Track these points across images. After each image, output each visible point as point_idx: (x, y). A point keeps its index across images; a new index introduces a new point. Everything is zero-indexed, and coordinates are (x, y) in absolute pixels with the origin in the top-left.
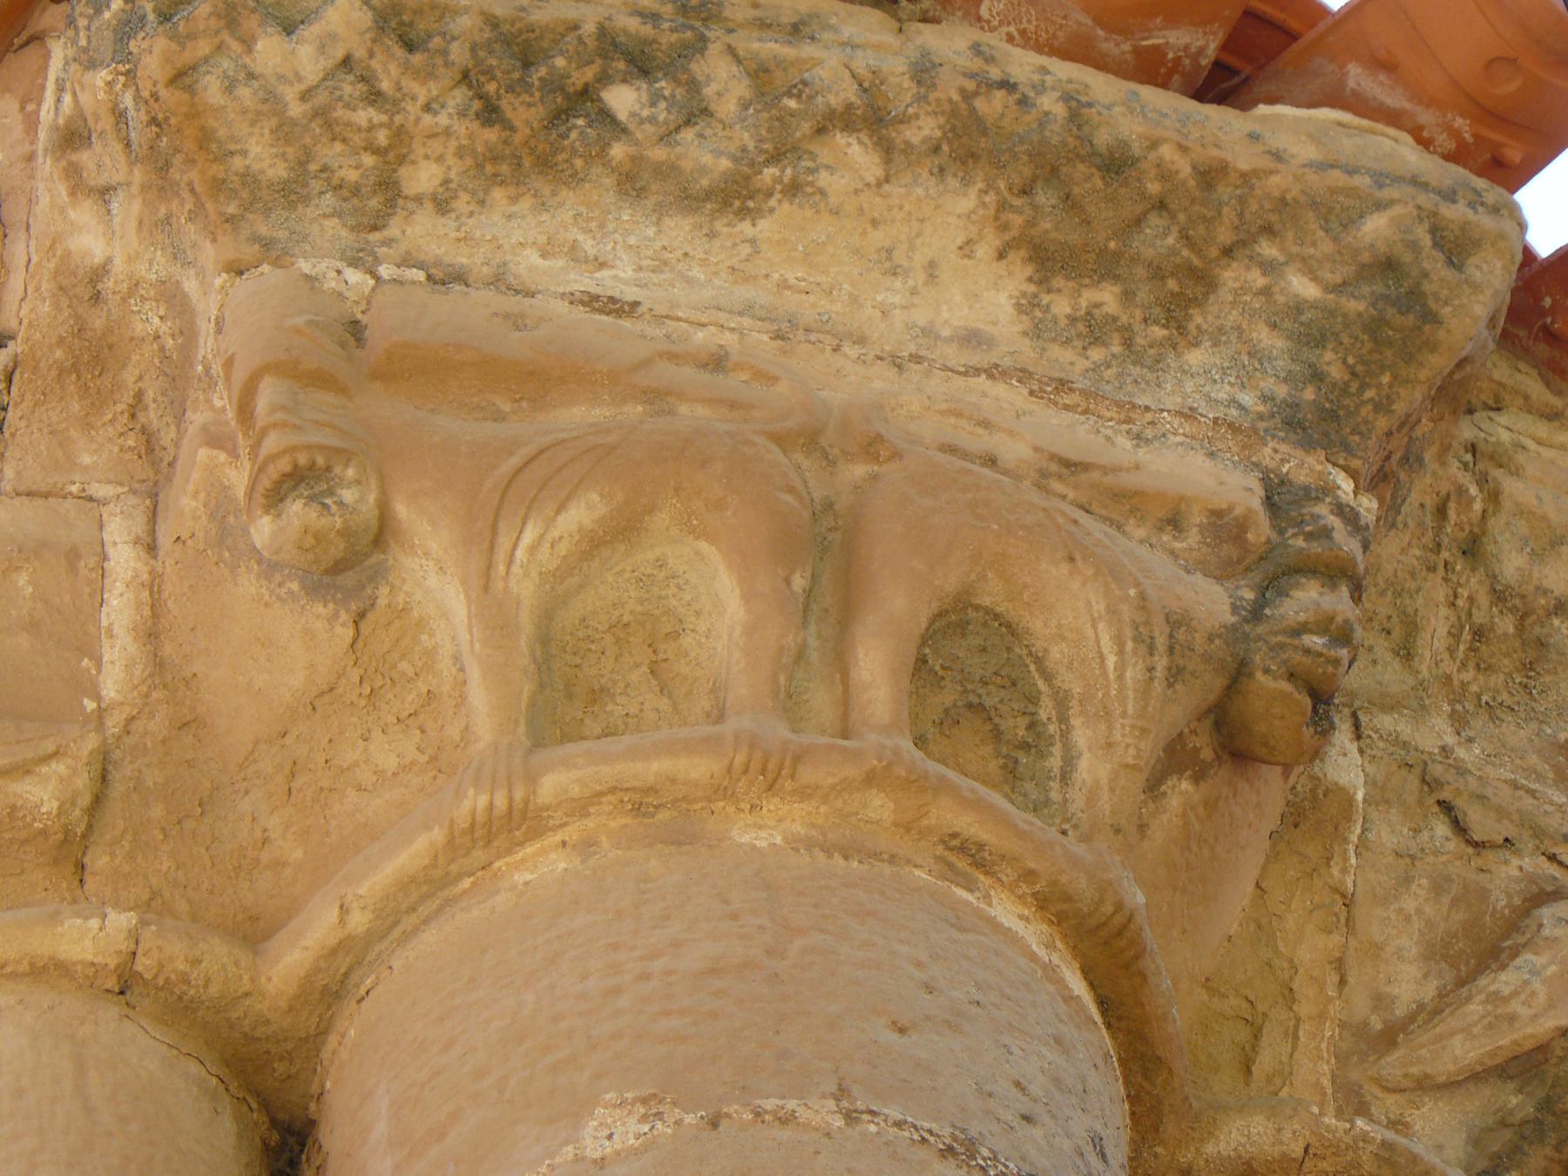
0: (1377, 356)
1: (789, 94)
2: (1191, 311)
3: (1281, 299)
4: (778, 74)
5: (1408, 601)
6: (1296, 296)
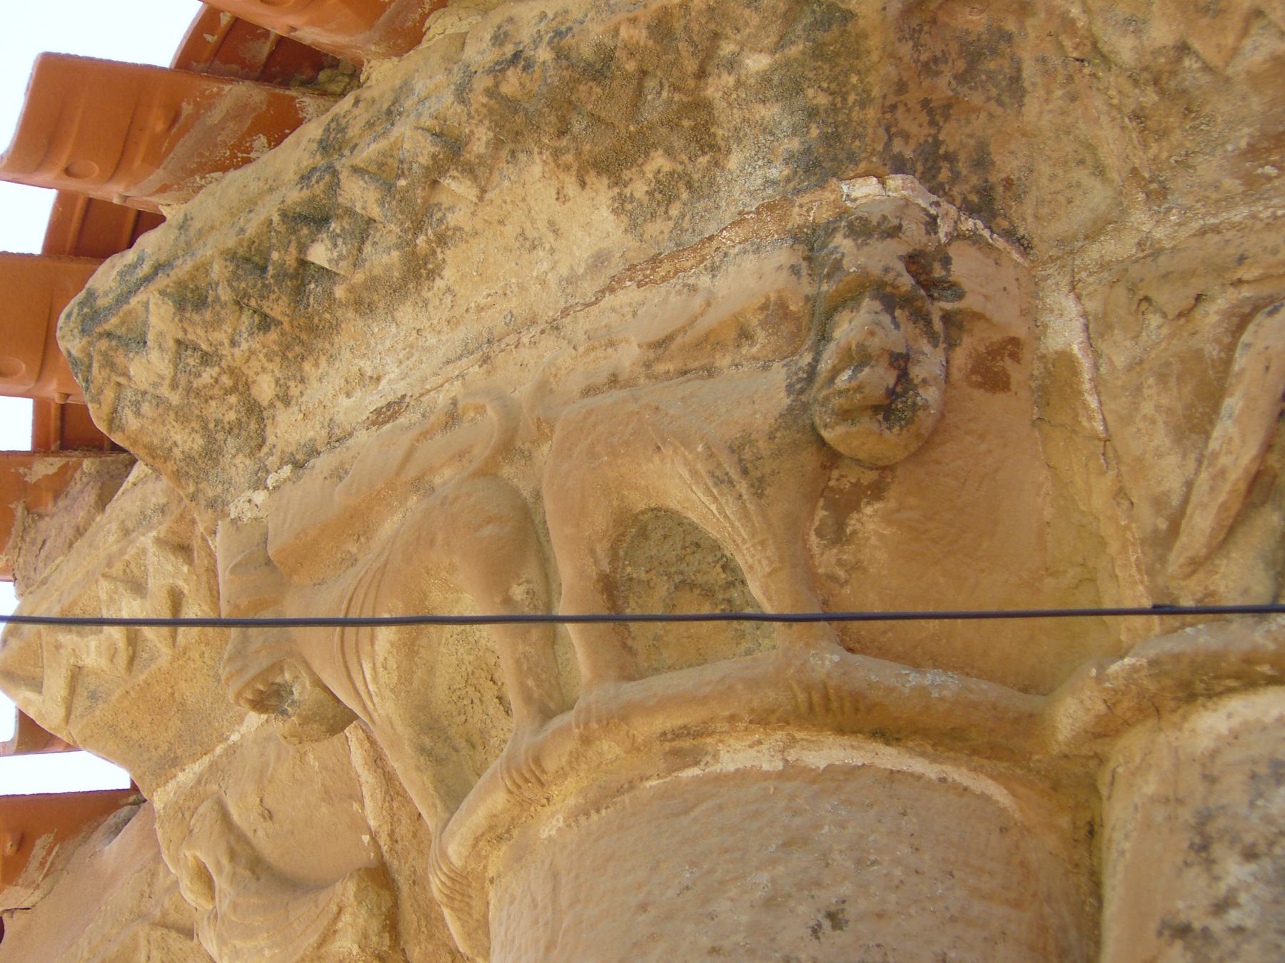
0: (838, 69)
1: (398, 177)
2: (712, 130)
3: (752, 81)
4: (390, 161)
6: (757, 73)
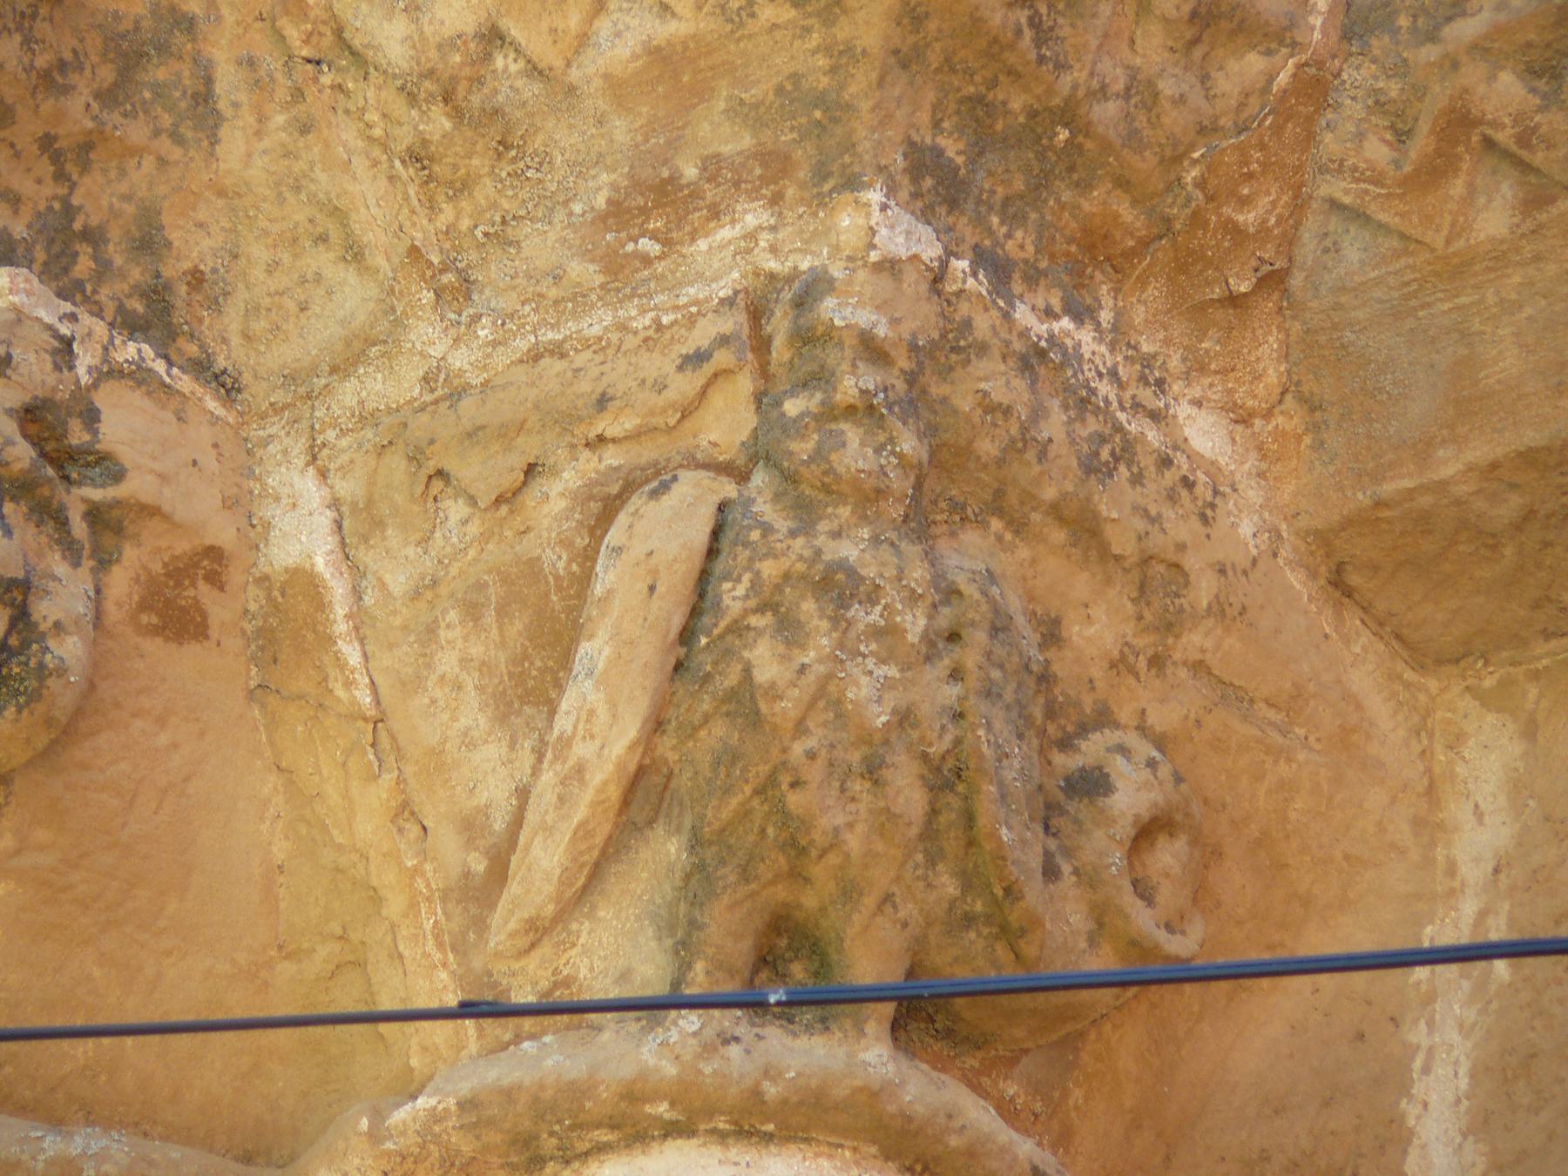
5: (313, 187)
